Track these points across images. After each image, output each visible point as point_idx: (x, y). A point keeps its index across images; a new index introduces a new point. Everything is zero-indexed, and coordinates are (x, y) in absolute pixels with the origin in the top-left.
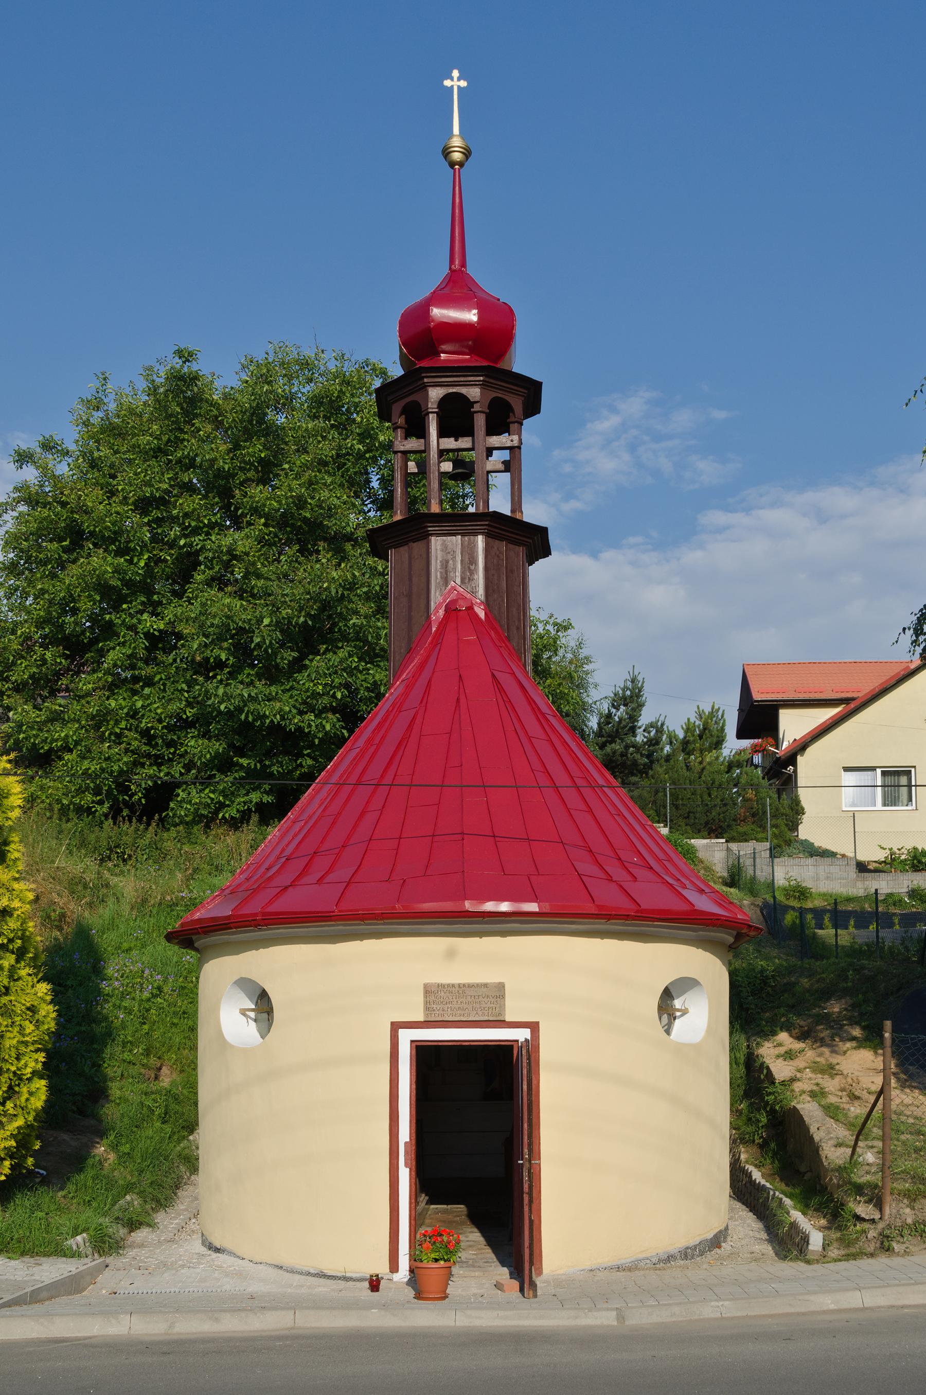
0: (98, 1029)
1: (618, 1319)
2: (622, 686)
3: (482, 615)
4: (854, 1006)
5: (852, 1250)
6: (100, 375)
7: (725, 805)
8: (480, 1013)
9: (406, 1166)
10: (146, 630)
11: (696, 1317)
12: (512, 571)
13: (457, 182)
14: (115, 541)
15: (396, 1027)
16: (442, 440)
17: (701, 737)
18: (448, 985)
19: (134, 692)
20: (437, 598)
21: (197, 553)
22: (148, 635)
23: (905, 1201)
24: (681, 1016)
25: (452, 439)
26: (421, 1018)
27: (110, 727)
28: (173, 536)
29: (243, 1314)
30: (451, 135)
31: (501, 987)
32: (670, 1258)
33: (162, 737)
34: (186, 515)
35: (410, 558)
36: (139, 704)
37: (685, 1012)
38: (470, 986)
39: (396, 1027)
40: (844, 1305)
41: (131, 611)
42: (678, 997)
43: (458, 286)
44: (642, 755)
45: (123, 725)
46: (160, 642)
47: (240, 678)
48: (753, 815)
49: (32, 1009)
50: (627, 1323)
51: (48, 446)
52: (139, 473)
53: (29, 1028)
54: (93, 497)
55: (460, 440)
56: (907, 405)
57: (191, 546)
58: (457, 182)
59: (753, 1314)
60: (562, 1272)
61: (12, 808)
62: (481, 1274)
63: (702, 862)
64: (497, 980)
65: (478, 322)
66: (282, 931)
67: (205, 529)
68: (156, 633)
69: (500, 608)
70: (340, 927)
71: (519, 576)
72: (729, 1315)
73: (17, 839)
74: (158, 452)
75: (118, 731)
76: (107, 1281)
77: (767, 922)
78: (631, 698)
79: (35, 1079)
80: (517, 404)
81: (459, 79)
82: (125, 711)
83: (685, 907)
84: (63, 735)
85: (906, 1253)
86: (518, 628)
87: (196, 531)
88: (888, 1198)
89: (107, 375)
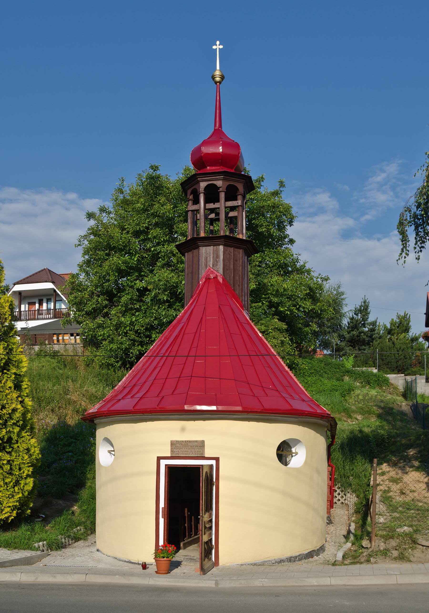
0: (87, 458)
1: (215, 584)
2: (360, 305)
3: (221, 280)
4: (419, 452)
5: (356, 560)
6: (121, 179)
7: (406, 358)
8: (194, 453)
9: (162, 517)
10: (137, 287)
11: (251, 585)
12: (236, 261)
13: (218, 91)
14: (124, 249)
15: (159, 459)
16: (207, 205)
17: (398, 327)
18: (181, 441)
19: (133, 315)
20: (203, 273)
21: (158, 253)
22: (138, 290)
23: (383, 540)
24: (295, 455)
25: (212, 204)
26: (169, 455)
27: (122, 329)
28: (148, 247)
29: (65, 575)
30: (215, 69)
31: (203, 442)
32: (281, 561)
33: (143, 333)
34: (155, 237)
35: (193, 256)
36: (134, 319)
37: (296, 454)
38: (190, 442)
39: (159, 459)
40: (322, 583)
41: (131, 280)
42: (294, 447)
43: (218, 135)
44: (367, 336)
45: (128, 328)
46: (143, 292)
47: (174, 307)
48: (420, 363)
49: (28, 450)
50: (219, 586)
51: (103, 210)
52: (135, 220)
53: (26, 457)
54: (116, 233)
55: (216, 204)
56: (415, 176)
57: (156, 251)
58: (218, 91)
59: (278, 585)
60: (228, 565)
61: (23, 367)
62: (193, 564)
63: (392, 385)
64: (201, 440)
65: (222, 152)
66: (117, 418)
67: (162, 243)
68: (142, 289)
69: (230, 277)
70: (137, 416)
71: (240, 262)
72: (266, 585)
73: (26, 380)
74: (145, 210)
75: (125, 331)
76: (45, 561)
77: (413, 413)
78: (364, 310)
79: (28, 478)
80: (241, 187)
81: (219, 45)
82: (129, 322)
83: (289, 408)
84: (102, 333)
85: (375, 563)
86: (239, 286)
87: (158, 244)
88: (374, 538)
89: (124, 179)
